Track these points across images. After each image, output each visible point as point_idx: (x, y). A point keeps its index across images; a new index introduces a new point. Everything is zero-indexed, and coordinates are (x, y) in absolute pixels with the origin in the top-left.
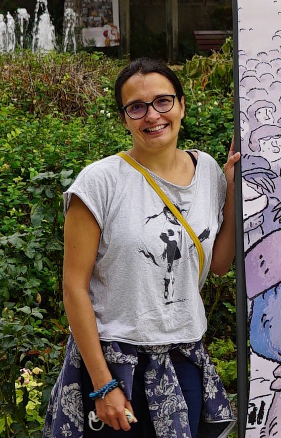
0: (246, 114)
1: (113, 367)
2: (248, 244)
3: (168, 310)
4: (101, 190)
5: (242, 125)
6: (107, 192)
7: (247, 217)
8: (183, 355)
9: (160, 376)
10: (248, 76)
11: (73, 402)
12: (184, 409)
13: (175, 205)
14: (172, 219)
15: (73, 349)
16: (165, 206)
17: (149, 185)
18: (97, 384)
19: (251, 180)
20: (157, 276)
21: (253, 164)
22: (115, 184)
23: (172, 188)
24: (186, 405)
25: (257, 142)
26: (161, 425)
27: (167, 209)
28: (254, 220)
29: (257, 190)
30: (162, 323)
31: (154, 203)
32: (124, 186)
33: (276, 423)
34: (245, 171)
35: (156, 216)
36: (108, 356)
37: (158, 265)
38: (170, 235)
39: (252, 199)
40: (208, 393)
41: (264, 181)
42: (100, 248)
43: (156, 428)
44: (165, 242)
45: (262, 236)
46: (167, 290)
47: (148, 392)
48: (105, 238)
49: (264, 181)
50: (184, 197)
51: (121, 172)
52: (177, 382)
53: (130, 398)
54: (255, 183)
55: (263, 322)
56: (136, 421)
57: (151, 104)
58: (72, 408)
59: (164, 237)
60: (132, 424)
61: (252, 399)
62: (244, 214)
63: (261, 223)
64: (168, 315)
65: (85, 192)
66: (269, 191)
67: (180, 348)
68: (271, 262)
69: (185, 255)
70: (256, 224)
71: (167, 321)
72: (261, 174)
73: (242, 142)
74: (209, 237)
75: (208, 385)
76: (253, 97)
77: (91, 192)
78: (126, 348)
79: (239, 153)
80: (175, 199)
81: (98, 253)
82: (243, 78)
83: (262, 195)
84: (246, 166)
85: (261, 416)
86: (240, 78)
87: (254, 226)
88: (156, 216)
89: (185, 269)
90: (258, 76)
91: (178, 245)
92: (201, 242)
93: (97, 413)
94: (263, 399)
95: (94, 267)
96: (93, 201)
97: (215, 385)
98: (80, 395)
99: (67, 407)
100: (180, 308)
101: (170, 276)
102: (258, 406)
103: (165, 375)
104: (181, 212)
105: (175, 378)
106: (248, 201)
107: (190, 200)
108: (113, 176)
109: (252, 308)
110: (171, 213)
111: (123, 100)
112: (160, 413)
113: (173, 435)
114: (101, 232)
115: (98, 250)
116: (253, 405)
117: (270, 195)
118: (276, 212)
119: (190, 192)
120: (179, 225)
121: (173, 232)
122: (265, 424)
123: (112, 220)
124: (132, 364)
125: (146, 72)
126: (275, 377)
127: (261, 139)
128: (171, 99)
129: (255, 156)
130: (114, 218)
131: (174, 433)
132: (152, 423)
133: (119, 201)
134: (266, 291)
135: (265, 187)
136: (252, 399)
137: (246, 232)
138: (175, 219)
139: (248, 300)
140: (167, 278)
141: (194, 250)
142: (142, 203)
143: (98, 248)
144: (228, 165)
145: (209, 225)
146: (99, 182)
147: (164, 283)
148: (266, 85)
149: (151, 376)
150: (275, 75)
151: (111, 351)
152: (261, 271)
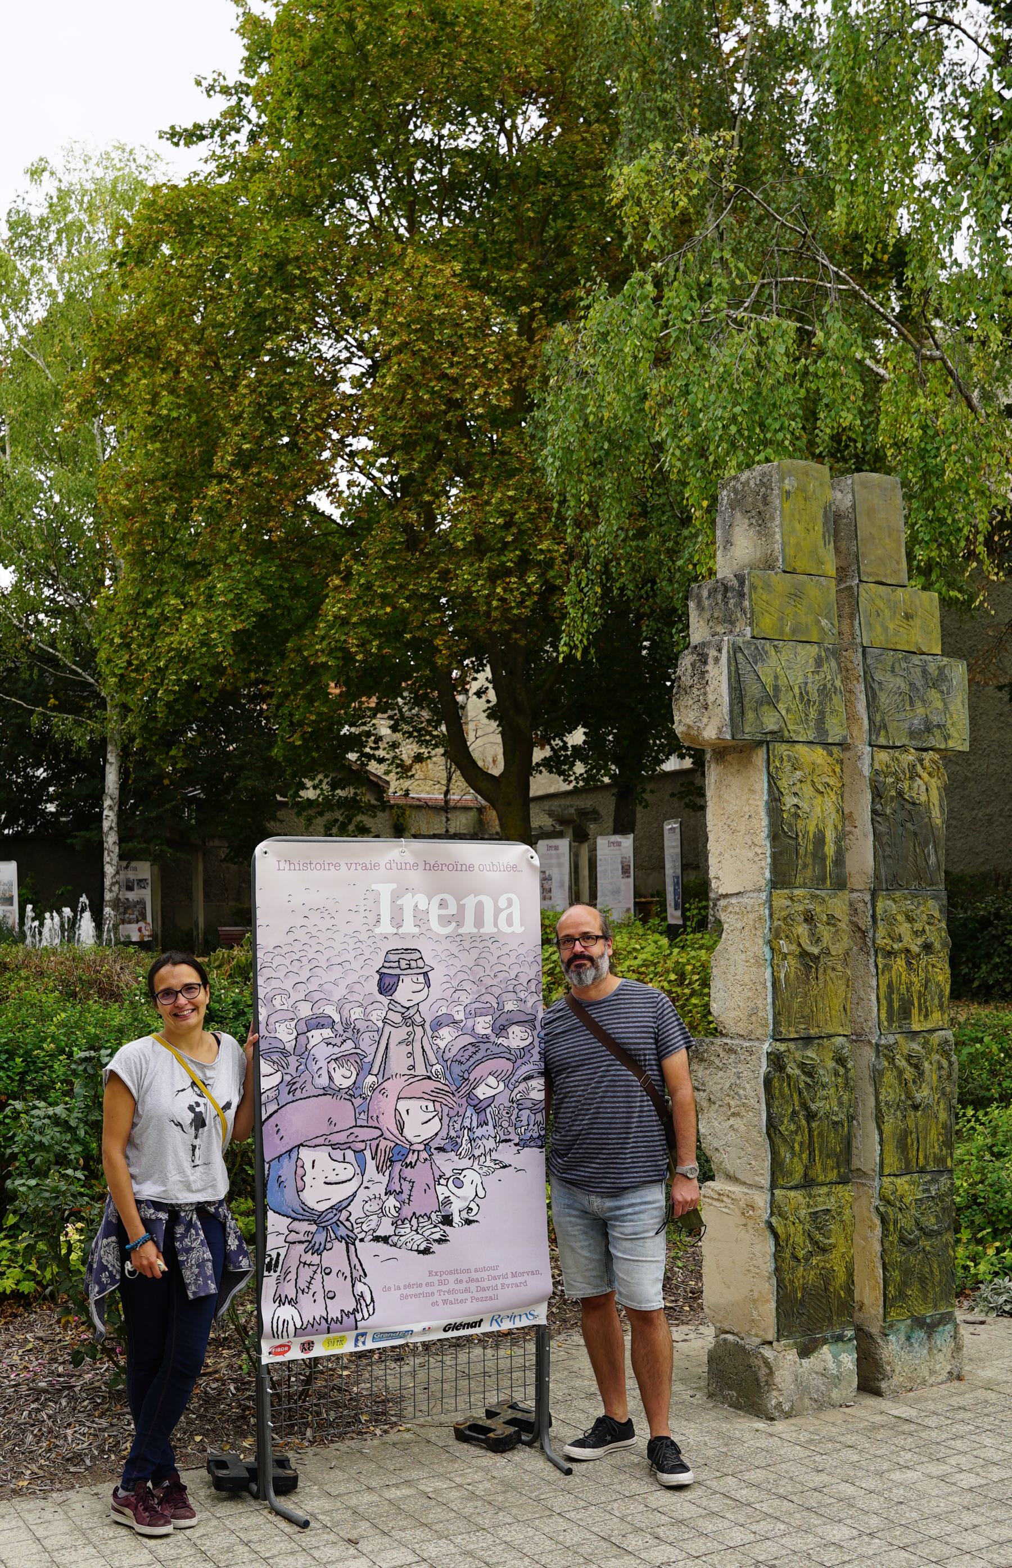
1: (146, 1222)
8: (208, 1212)
9: (187, 1230)
47: (177, 1244)
50: (209, 1073)
59: (191, 1108)
60: (163, 1272)
78: (157, 1206)
80: (201, 1075)
85: (276, 1266)
89: (210, 1136)
101: (197, 1142)
102: (274, 1256)
105: (201, 1232)
114: (136, 1103)
125: (175, 964)
141: (218, 1119)
148: (281, 975)
149: (180, 1230)
152: (277, 1138)
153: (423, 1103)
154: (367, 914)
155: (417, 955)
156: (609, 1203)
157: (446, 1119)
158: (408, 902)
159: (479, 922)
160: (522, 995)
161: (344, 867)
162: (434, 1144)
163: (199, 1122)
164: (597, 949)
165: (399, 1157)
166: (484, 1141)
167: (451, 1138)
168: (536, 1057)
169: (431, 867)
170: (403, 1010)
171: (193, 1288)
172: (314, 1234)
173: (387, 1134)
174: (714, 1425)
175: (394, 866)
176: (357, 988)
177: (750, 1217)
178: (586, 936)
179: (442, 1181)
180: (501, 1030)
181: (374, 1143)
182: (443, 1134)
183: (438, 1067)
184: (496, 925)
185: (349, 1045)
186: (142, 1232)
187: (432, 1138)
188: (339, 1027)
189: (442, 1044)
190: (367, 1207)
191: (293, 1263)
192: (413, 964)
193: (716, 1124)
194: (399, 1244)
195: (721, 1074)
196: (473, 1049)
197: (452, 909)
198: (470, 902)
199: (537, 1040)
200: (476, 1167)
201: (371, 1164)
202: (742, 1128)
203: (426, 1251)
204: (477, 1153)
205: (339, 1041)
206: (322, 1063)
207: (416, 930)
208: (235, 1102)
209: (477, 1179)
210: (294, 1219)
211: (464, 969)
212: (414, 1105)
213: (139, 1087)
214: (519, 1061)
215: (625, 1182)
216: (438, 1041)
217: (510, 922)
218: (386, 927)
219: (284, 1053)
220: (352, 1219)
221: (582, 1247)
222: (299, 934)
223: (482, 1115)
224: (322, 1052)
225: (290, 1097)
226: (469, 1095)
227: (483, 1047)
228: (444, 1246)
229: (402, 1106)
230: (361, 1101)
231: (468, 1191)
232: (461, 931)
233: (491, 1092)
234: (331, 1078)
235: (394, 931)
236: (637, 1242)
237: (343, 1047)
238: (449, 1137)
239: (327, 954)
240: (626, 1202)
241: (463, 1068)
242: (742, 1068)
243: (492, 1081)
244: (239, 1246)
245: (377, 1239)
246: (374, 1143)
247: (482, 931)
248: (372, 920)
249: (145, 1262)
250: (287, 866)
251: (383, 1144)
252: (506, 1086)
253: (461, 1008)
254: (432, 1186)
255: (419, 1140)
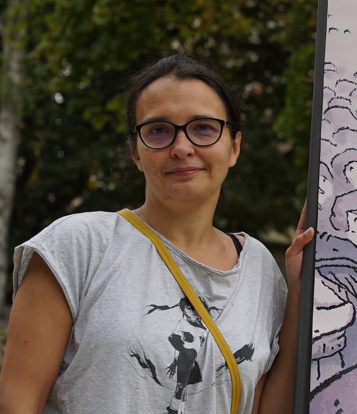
0: (329, 166)
2: (318, 379)
4: (80, 253)
7: (318, 334)
10: (337, 107)
13: (200, 297)
16: (183, 297)
17: (161, 260)
19: (330, 277)
21: (334, 250)
22: (106, 247)
23: (198, 270)
25: (343, 216)
27: (186, 303)
28: (331, 342)
29: (338, 293)
32: (119, 253)
34: (321, 260)
35: (165, 308)
37: (160, 384)
38: (186, 340)
39: (328, 306)
42: (67, 353)
44: (176, 348)
45: (341, 369)
48: (76, 334)
50: (217, 289)
51: (116, 232)
54: (335, 280)
57: (184, 128)
59: (175, 341)
63: (341, 347)
65: (53, 252)
70: (333, 348)
72: (347, 268)
73: (316, 253)
76: (343, 141)
77: (64, 253)
79: (311, 229)
80: (202, 290)
81: (63, 362)
82: (329, 108)
83: (345, 303)
86: (325, 107)
87: (329, 352)
88: (165, 308)
91: (198, 359)
92: (238, 363)
96: (64, 268)
104: (209, 311)
106: (322, 310)
108: (103, 235)
110: (193, 309)
111: (138, 115)
114: (73, 322)
115: (64, 356)
119: (228, 283)
120: (205, 329)
121: (192, 337)
123: (91, 304)
125: (183, 76)
127: (351, 211)
128: (217, 126)
129: (339, 238)
130: (96, 301)
133: (106, 274)
135: (352, 291)
137: (315, 360)
138: (197, 319)
141: (226, 374)
142: (146, 282)
143: (65, 351)
144: (292, 249)
146: (77, 239)
174: (186, 69)
213: (82, 292)
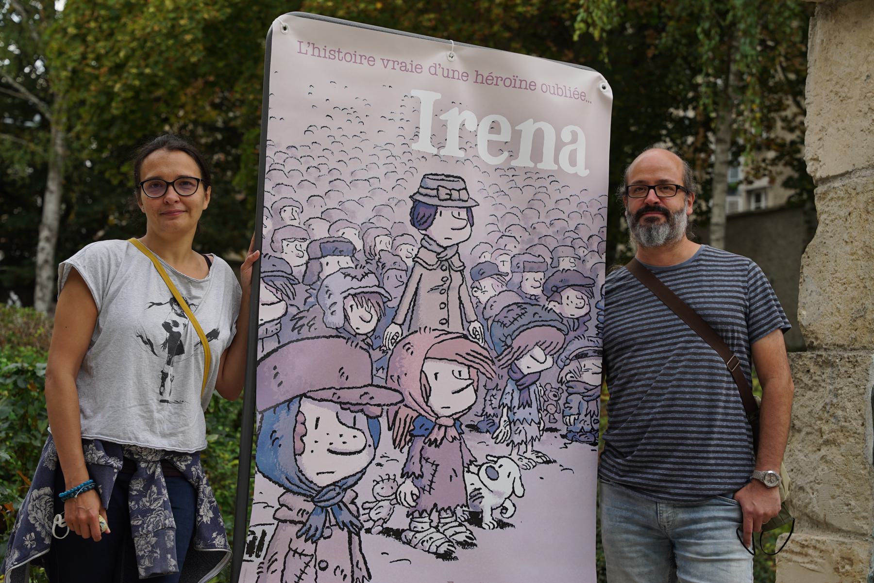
0: (270, 209)
1: (92, 468)
3: (162, 409)
4: (102, 268)
5: (265, 221)
6: (109, 271)
7: (263, 322)
8: (176, 469)
9: (147, 487)
11: (42, 508)
12: (172, 527)
14: (179, 312)
15: (49, 449)
18: (70, 482)
20: (154, 367)
22: (120, 263)
24: (174, 522)
26: (143, 542)
27: (174, 301)
30: (153, 423)
31: (160, 291)
33: (276, 560)
34: (265, 272)
35: (160, 304)
36: (89, 456)
37: (154, 353)
40: (202, 516)
41: (284, 286)
43: (136, 545)
45: (278, 345)
46: (163, 385)
47: (132, 504)
48: (100, 322)
49: (284, 286)
50: (195, 292)
51: (127, 254)
52: (167, 496)
53: (107, 506)
55: (273, 439)
56: (109, 531)
57: (172, 184)
58: (40, 515)
59: (167, 326)
60: (104, 534)
61: (254, 526)
62: (260, 318)
64: (162, 414)
66: (289, 298)
67: (175, 460)
68: (286, 375)
69: (189, 351)
71: (160, 421)
74: (219, 338)
75: (203, 507)
78: (111, 448)
80: (184, 293)
82: (270, 171)
83: (281, 301)
84: (266, 266)
85: (260, 548)
86: (267, 170)
87: (269, 334)
88: (160, 304)
89: (187, 367)
90: (286, 171)
91: (182, 339)
93: (65, 516)
94: (265, 528)
95: (83, 360)
97: (210, 508)
98: (51, 501)
99: (34, 514)
100: (177, 411)
101: (170, 370)
102: (259, 535)
103: (153, 486)
104: (189, 306)
105: (165, 492)
107: (201, 296)
108: (118, 255)
109: (261, 422)
110: (178, 305)
111: (142, 175)
112: (143, 529)
113: (155, 555)
114: (98, 314)
115: (92, 336)
116: (253, 533)
117: (289, 302)
118: (295, 321)
122: (264, 559)
123: (110, 301)
124: (115, 468)
125: (172, 149)
126: (280, 504)
128: (195, 182)
131: (156, 552)
132: (133, 540)
134: (278, 405)
136: (254, 526)
139: (257, 413)
140: (166, 371)
141: (201, 349)
144: (245, 265)
145: (219, 325)
146: (101, 258)
147: (160, 376)
148: (294, 183)
149: (137, 486)
150: (304, 173)
151: (92, 450)
152: (274, 384)
153: (457, 368)
154: (403, 124)
155: (460, 185)
156: (683, 515)
157: (482, 392)
158: (453, 118)
159: (537, 154)
160: (581, 252)
161: (379, 63)
162: (466, 420)
163: (175, 346)
164: (676, 202)
165: (422, 431)
166: (526, 426)
167: (488, 416)
168: (593, 332)
169: (483, 80)
170: (439, 250)
171: (147, 563)
172: (310, 515)
173: (409, 401)
175: (439, 71)
176: (386, 211)
177: (847, 574)
178: (663, 185)
179: (473, 468)
180: (553, 291)
181: (392, 409)
182: (478, 409)
183: (477, 325)
184: (556, 161)
185: (371, 280)
186: (84, 477)
187: (465, 412)
188: (360, 256)
189: (483, 298)
190: (378, 489)
191: (280, 548)
192: (455, 195)
193: (801, 456)
194: (415, 541)
195: (810, 394)
196: (519, 311)
197: (505, 136)
198: (528, 128)
199: (594, 311)
200: (514, 456)
201: (386, 436)
202: (839, 459)
203: (447, 556)
204: (517, 439)
205: (359, 273)
206: (337, 298)
207: (461, 154)
208: (225, 334)
209: (516, 473)
210: (288, 490)
211: (514, 211)
212: (445, 368)
214: (572, 334)
215: (706, 488)
216: (479, 294)
217: (573, 162)
218: (424, 145)
219: (290, 278)
220: (359, 502)
221: (640, 575)
222: (319, 135)
223: (525, 394)
224: (338, 285)
225: (295, 335)
226: (512, 367)
227: (531, 310)
228: (469, 551)
229: (430, 367)
230: (380, 354)
231: (503, 485)
232: (514, 163)
233: (537, 367)
234: (346, 317)
235: (434, 151)
236: (719, 565)
237: (365, 282)
238: (484, 414)
239: (353, 166)
240: (706, 515)
241: (507, 331)
242: (840, 382)
243: (538, 353)
244: (214, 520)
245: (387, 532)
246: (392, 409)
247: (539, 166)
248: (409, 132)
249: (83, 516)
250: (310, 50)
251: (403, 412)
252: (555, 362)
253: (508, 258)
254: (460, 473)
255: (448, 412)
